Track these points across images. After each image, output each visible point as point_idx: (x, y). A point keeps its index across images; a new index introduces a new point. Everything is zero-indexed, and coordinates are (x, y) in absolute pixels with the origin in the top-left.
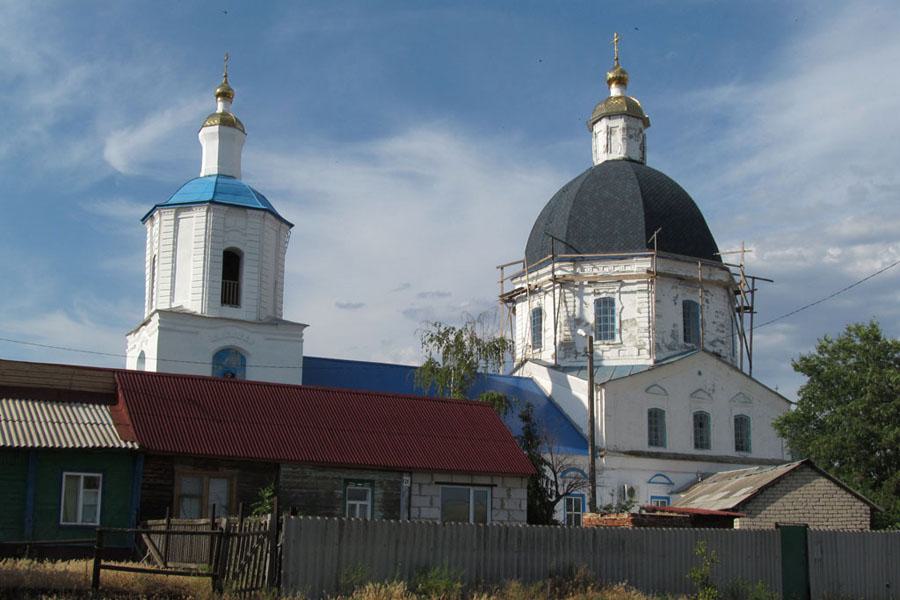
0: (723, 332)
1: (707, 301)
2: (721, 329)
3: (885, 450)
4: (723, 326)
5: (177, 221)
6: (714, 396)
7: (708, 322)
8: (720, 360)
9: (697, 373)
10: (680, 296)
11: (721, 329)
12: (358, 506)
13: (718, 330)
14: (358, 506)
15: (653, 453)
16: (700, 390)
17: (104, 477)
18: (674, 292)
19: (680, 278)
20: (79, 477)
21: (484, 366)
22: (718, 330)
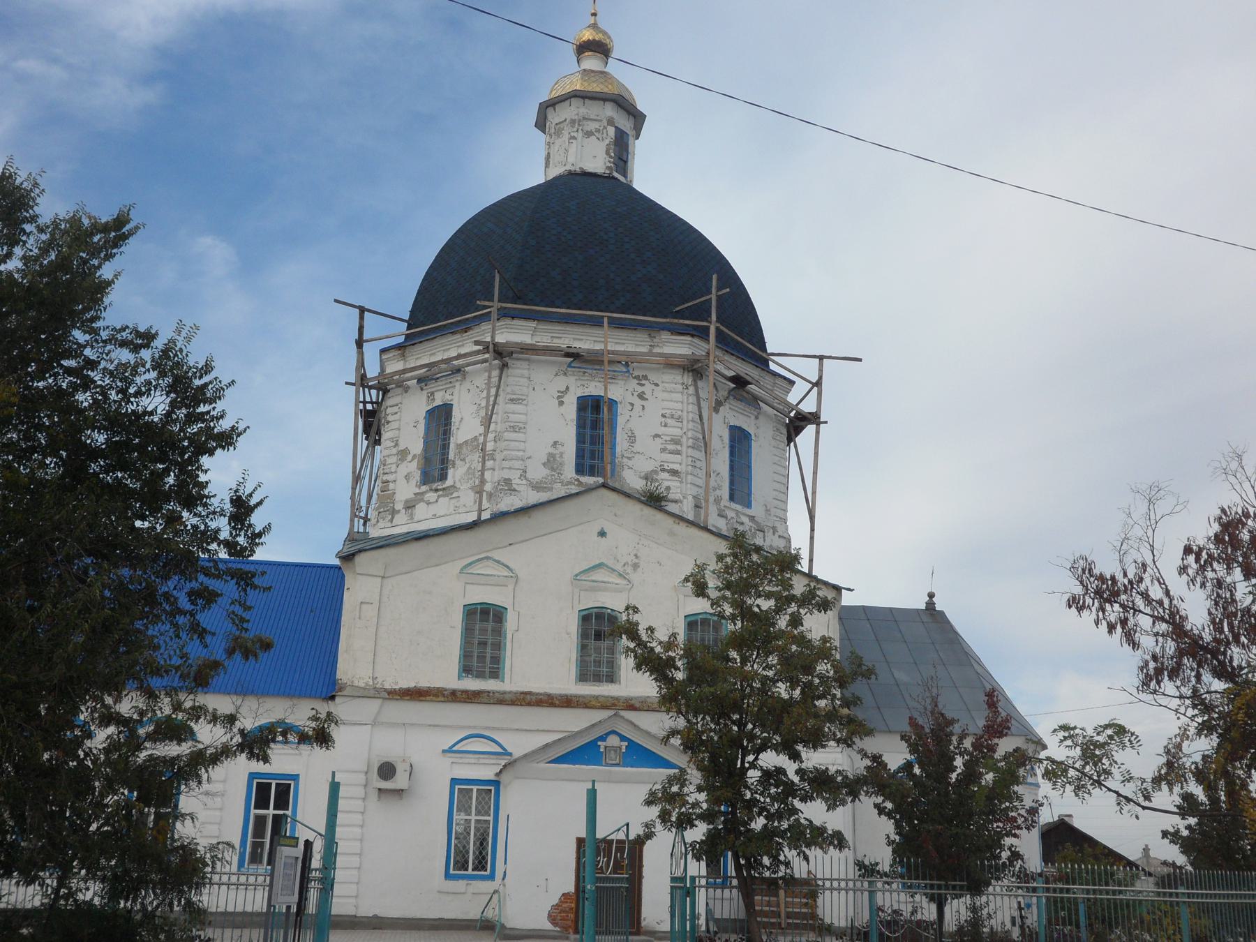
0: (678, 453)
1: (641, 396)
2: (671, 447)
3: (823, 839)
4: (676, 442)
5: (381, 707)
6: (635, 577)
7: (643, 434)
8: (660, 509)
9: (598, 529)
10: (572, 389)
11: (671, 447)
12: (475, 791)
13: (663, 450)
14: (475, 791)
15: (465, 692)
16: (600, 566)
17: (457, 784)
18: (561, 382)
19: (574, 356)
20: (472, 790)
21: (98, 221)
22: (663, 450)
